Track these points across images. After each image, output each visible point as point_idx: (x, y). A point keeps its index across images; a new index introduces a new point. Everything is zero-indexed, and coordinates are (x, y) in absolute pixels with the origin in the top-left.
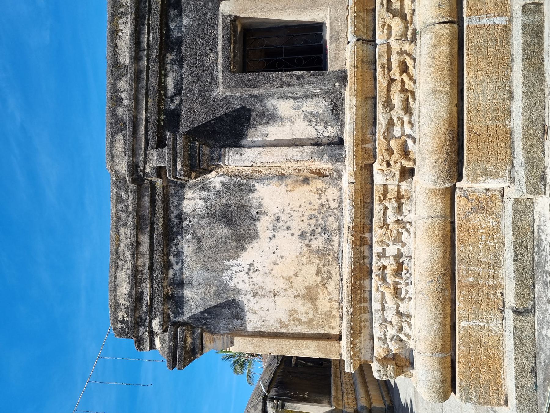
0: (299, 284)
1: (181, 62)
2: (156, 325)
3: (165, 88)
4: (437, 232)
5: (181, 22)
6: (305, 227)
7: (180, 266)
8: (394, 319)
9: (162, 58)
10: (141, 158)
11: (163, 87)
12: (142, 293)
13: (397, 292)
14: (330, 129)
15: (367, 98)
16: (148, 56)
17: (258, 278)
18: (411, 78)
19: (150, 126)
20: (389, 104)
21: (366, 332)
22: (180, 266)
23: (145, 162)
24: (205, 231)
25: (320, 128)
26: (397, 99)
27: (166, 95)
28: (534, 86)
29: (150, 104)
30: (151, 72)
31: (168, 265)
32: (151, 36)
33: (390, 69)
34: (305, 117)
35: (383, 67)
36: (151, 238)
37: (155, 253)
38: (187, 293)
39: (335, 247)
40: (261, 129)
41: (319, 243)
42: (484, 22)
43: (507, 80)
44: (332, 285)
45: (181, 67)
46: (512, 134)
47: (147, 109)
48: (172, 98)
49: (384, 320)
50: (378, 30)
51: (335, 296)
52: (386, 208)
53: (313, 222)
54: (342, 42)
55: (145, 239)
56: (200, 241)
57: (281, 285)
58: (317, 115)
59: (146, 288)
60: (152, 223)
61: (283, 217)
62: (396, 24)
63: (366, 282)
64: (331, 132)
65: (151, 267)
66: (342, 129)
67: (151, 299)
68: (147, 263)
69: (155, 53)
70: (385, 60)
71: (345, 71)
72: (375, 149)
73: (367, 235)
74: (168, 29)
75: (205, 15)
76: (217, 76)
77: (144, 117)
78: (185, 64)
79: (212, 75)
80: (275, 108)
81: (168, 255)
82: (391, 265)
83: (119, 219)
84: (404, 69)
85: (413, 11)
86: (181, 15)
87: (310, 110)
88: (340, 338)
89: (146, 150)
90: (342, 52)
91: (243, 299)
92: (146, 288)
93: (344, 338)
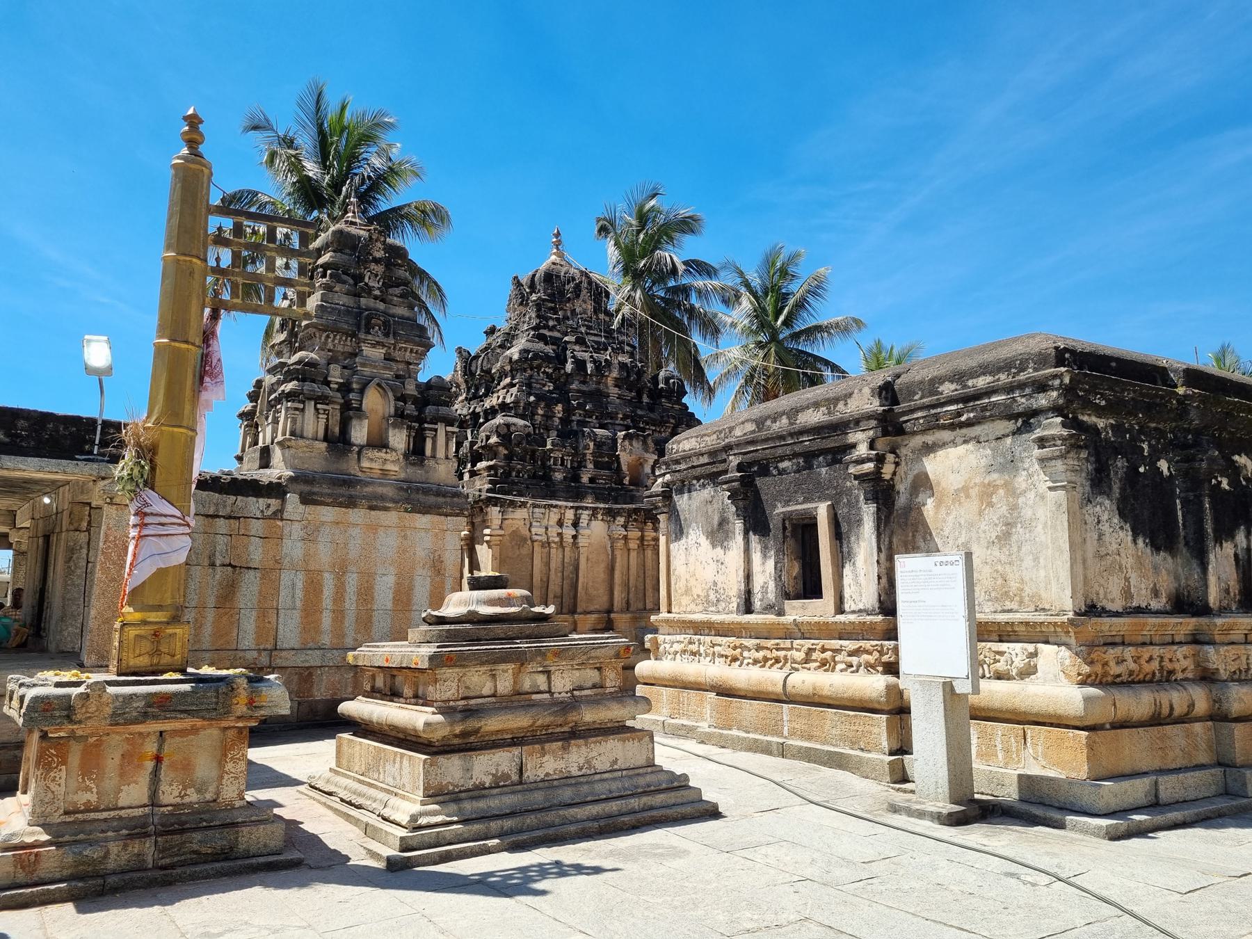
0: (692, 582)
1: (798, 471)
2: (668, 477)
3: (782, 461)
4: (699, 679)
5: (823, 467)
6: (719, 585)
7: (698, 488)
8: (672, 650)
9: (795, 455)
10: (736, 452)
11: (782, 459)
12: (680, 464)
13: (684, 652)
14: (759, 603)
15: (1193, 635)
16: (794, 443)
17: (693, 551)
18: (772, 665)
19: (754, 454)
20: (759, 648)
21: (671, 630)
22: (698, 488)
23: (735, 455)
24: (715, 506)
25: (759, 596)
26: (760, 655)
27: (778, 462)
28: (742, 744)
29: (767, 451)
30: (785, 447)
31: (698, 479)
32: (807, 443)
33: (777, 649)
34: (765, 583)
35: (777, 644)
36: (708, 464)
37: (699, 468)
38: (686, 496)
39: (711, 609)
40: (759, 547)
41: (712, 597)
42: (785, 719)
43: (756, 731)
44: (693, 607)
45: (795, 472)
46: (730, 729)
47: (763, 449)
48: (776, 467)
49: (673, 643)
50: (813, 641)
51: (688, 609)
52: (871, 653)
53: (722, 591)
54: (801, 611)
55: (705, 460)
56: (711, 502)
57: (691, 568)
58: (767, 593)
59: (683, 466)
60: (714, 463)
61: (723, 567)
62: (800, 656)
63: (692, 631)
64: (757, 604)
65: (693, 467)
66: (759, 613)
67: (679, 471)
68: (695, 464)
69: (797, 449)
70: (782, 646)
71: (784, 615)
72: (742, 637)
73: (713, 633)
74: (818, 456)
75: (828, 489)
76: (789, 505)
77: (759, 448)
78: (797, 475)
79: (790, 501)
80: (770, 557)
81: (703, 478)
82: (694, 648)
83: (721, 432)
84: (777, 661)
85: (809, 669)
86: (828, 466)
87: (770, 586)
88: (669, 612)
89: (741, 453)
90: (795, 612)
91: (683, 541)
92: (683, 466)
93: (670, 615)
